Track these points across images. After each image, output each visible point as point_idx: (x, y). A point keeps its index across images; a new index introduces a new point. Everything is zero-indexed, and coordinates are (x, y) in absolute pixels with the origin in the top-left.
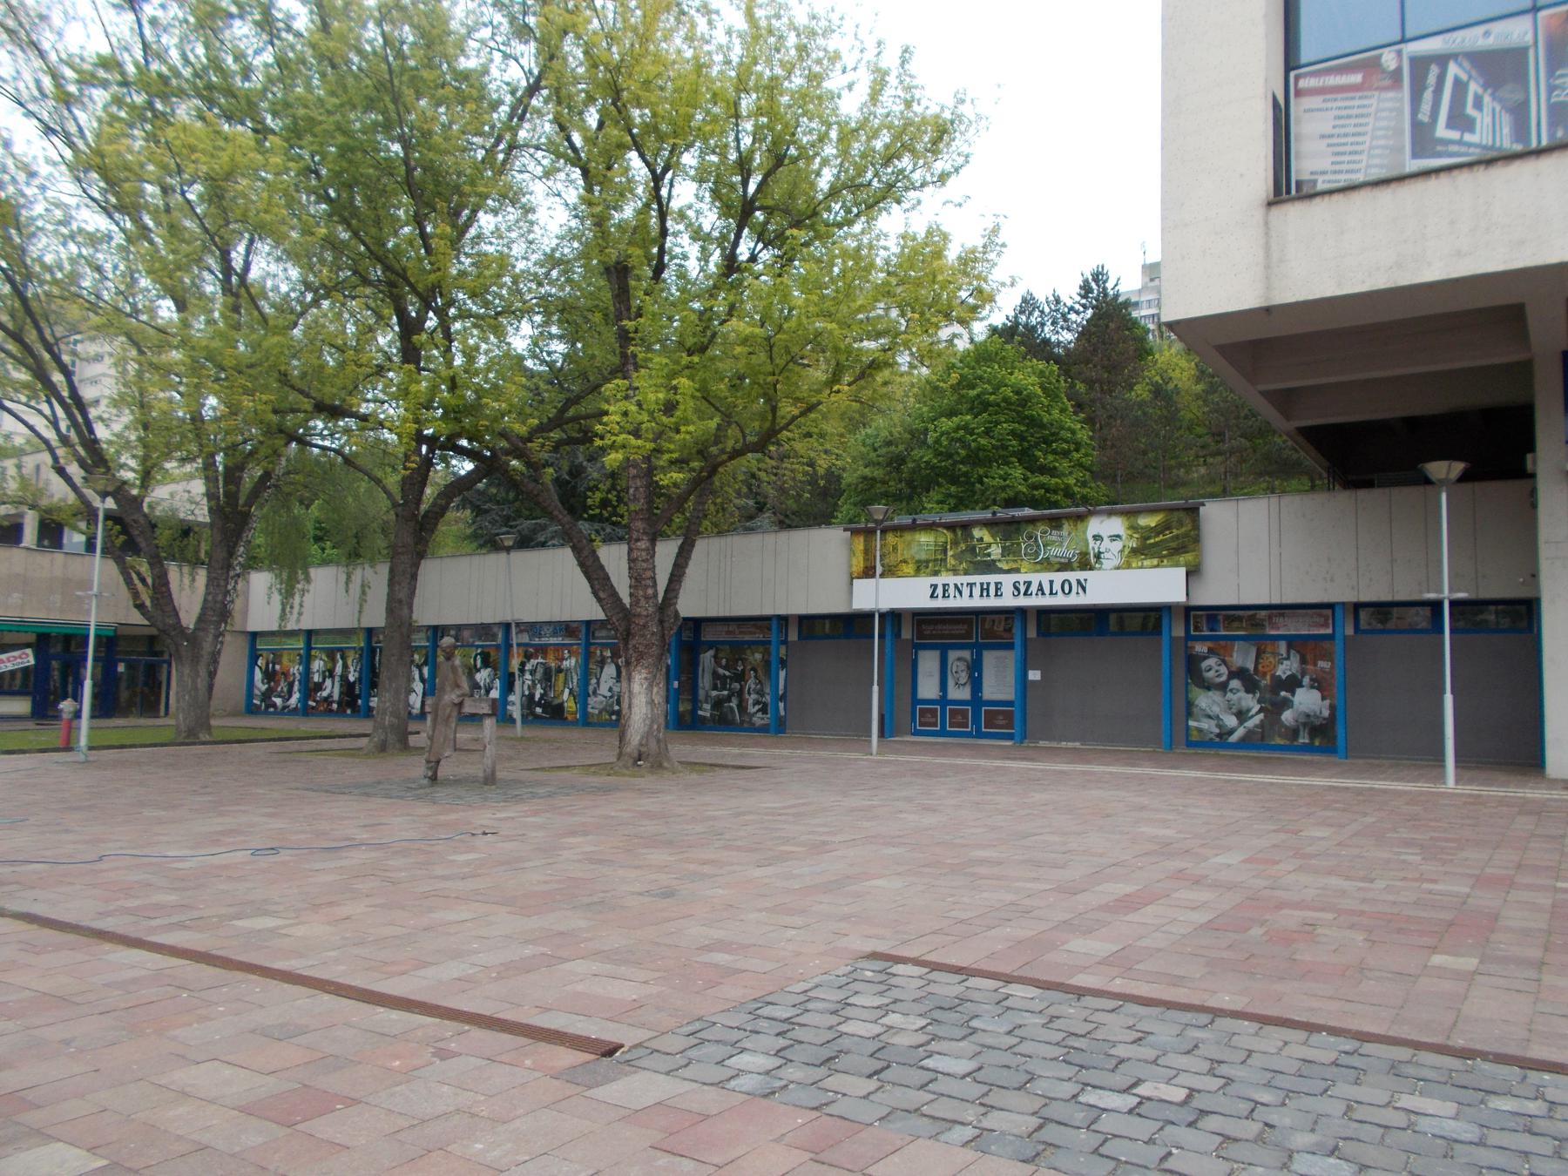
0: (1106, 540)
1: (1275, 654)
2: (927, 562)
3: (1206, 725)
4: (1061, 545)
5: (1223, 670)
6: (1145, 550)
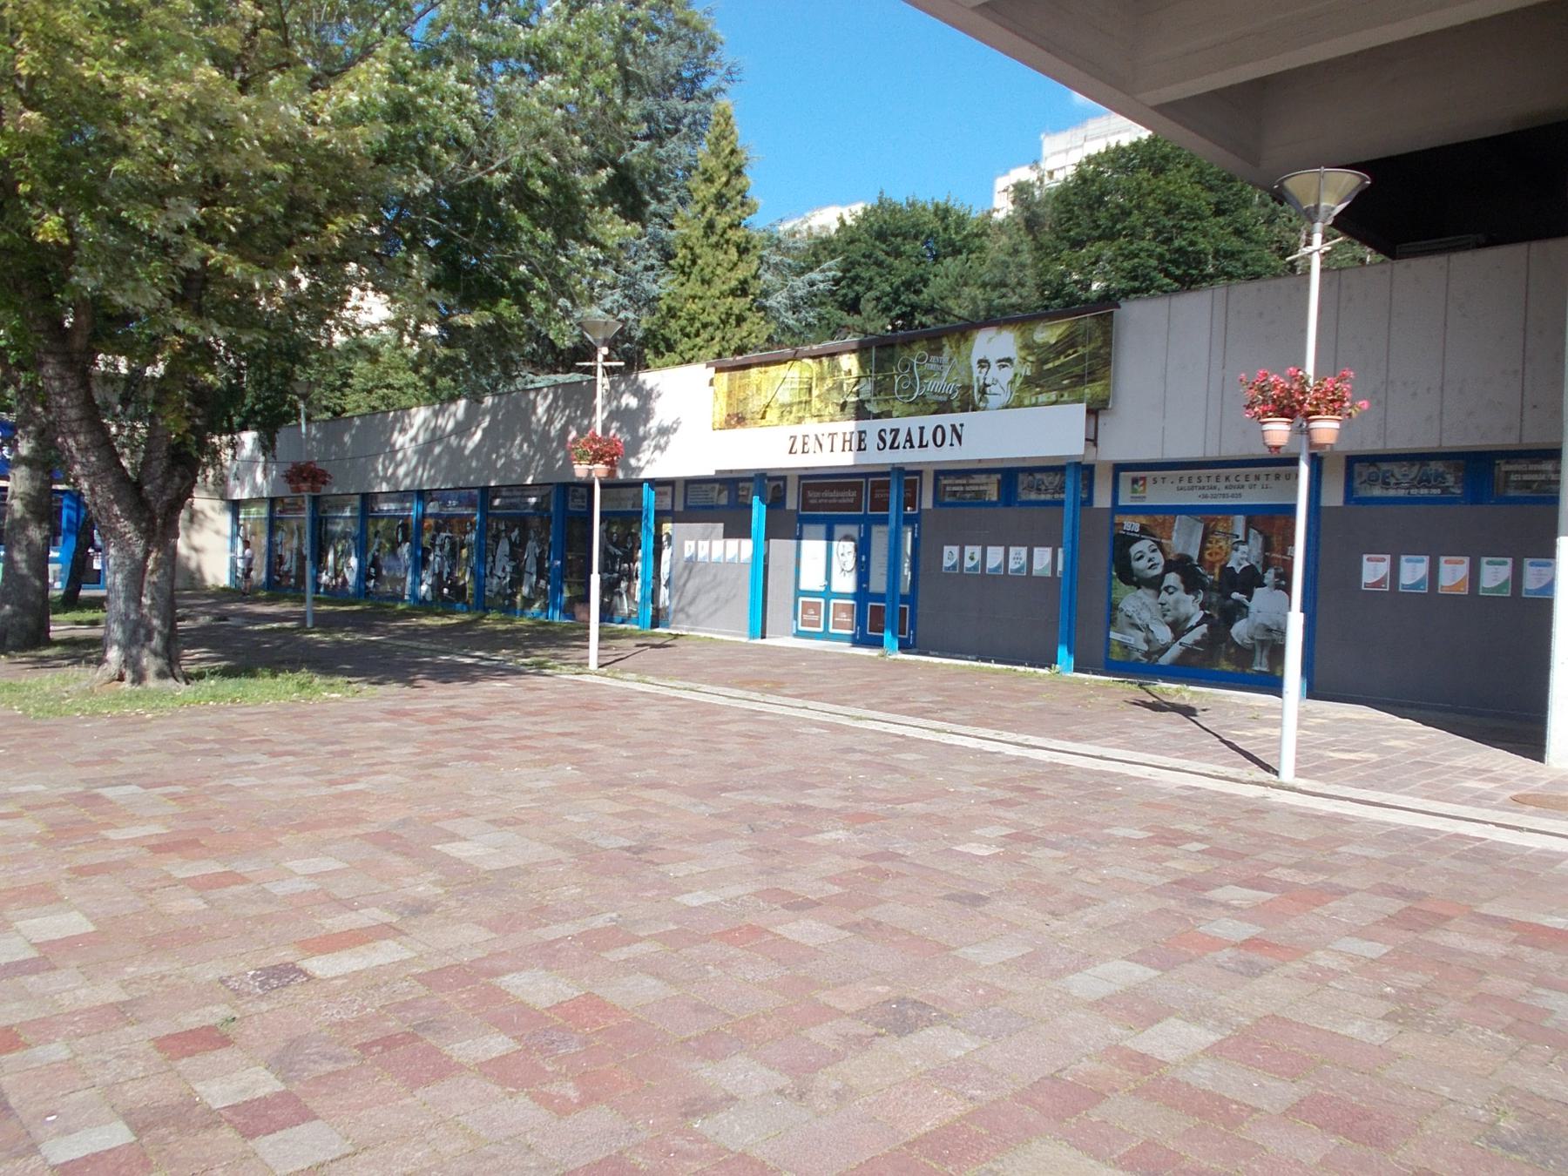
0: (994, 366)
1: (1228, 535)
2: (791, 405)
3: (1136, 639)
4: (940, 377)
5: (1159, 558)
6: (1047, 378)
